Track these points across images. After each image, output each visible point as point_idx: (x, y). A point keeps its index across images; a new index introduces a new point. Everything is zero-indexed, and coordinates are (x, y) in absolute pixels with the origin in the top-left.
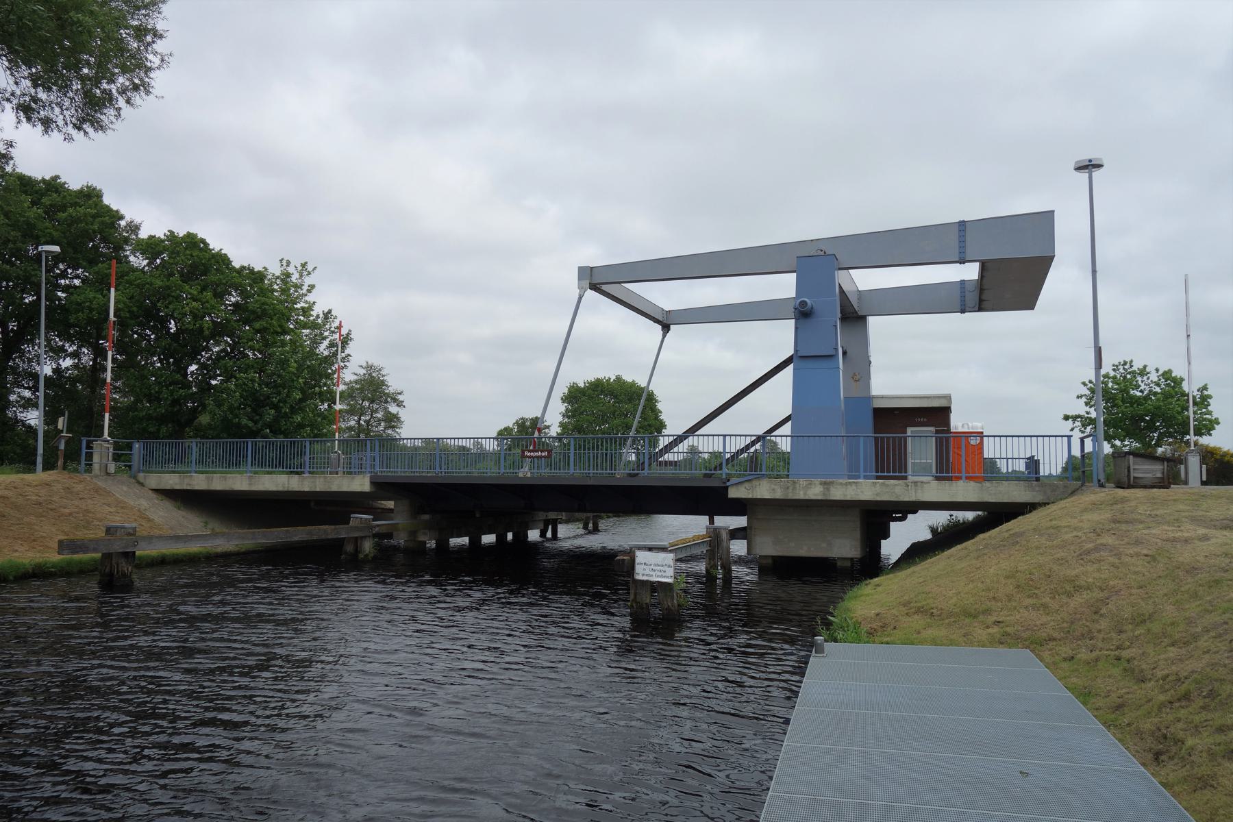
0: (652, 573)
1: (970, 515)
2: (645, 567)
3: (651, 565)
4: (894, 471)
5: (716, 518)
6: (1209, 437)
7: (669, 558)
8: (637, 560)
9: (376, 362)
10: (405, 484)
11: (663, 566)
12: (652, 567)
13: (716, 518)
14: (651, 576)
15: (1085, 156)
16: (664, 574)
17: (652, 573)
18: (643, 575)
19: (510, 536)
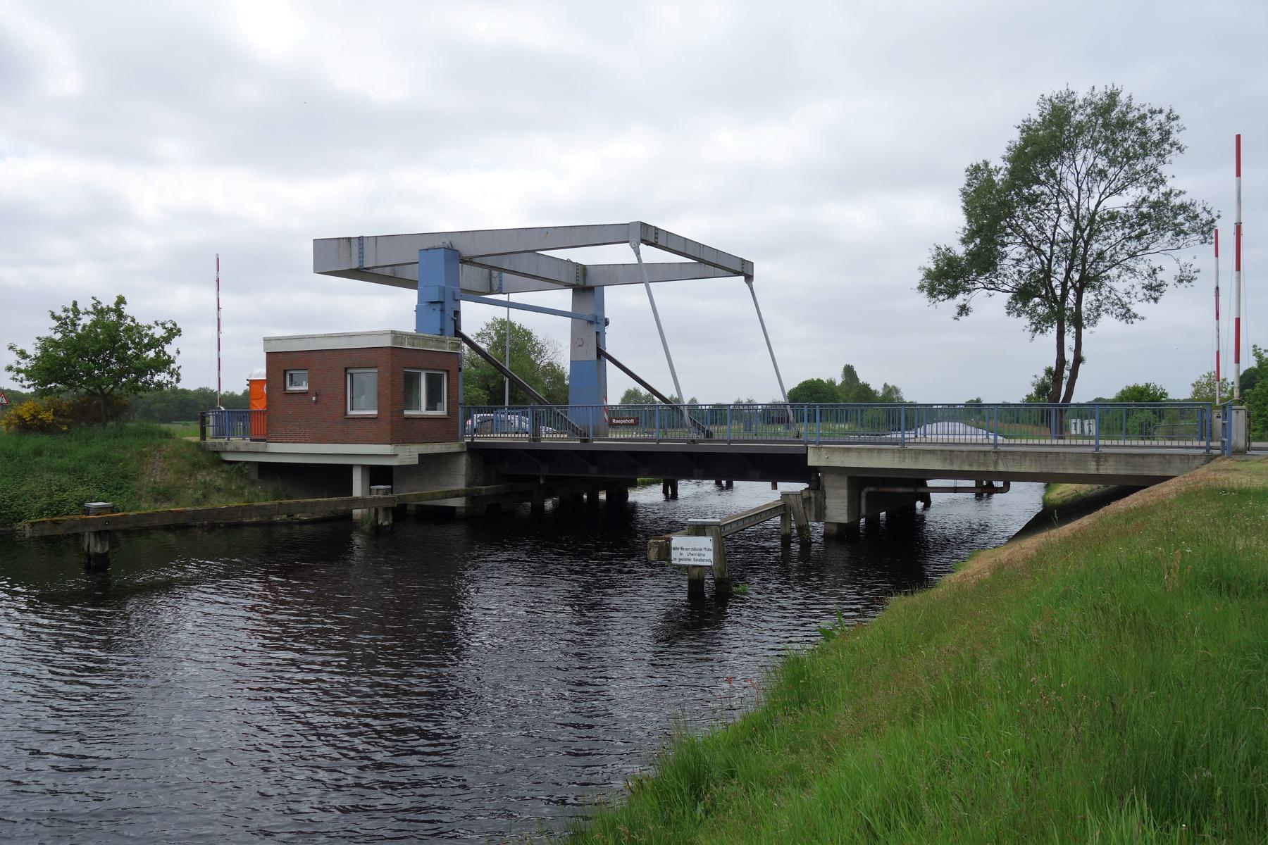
0: (689, 557)
1: (1084, 489)
2: (683, 552)
3: (688, 549)
4: (1043, 410)
5: (779, 484)
6: (888, 384)
7: (706, 542)
8: (673, 545)
9: (119, 294)
10: (484, 450)
11: (701, 550)
12: (690, 551)
13: (779, 484)
14: (689, 560)
15: (1163, 267)
16: (703, 558)
17: (690, 557)
18: (680, 560)
19: (603, 496)
